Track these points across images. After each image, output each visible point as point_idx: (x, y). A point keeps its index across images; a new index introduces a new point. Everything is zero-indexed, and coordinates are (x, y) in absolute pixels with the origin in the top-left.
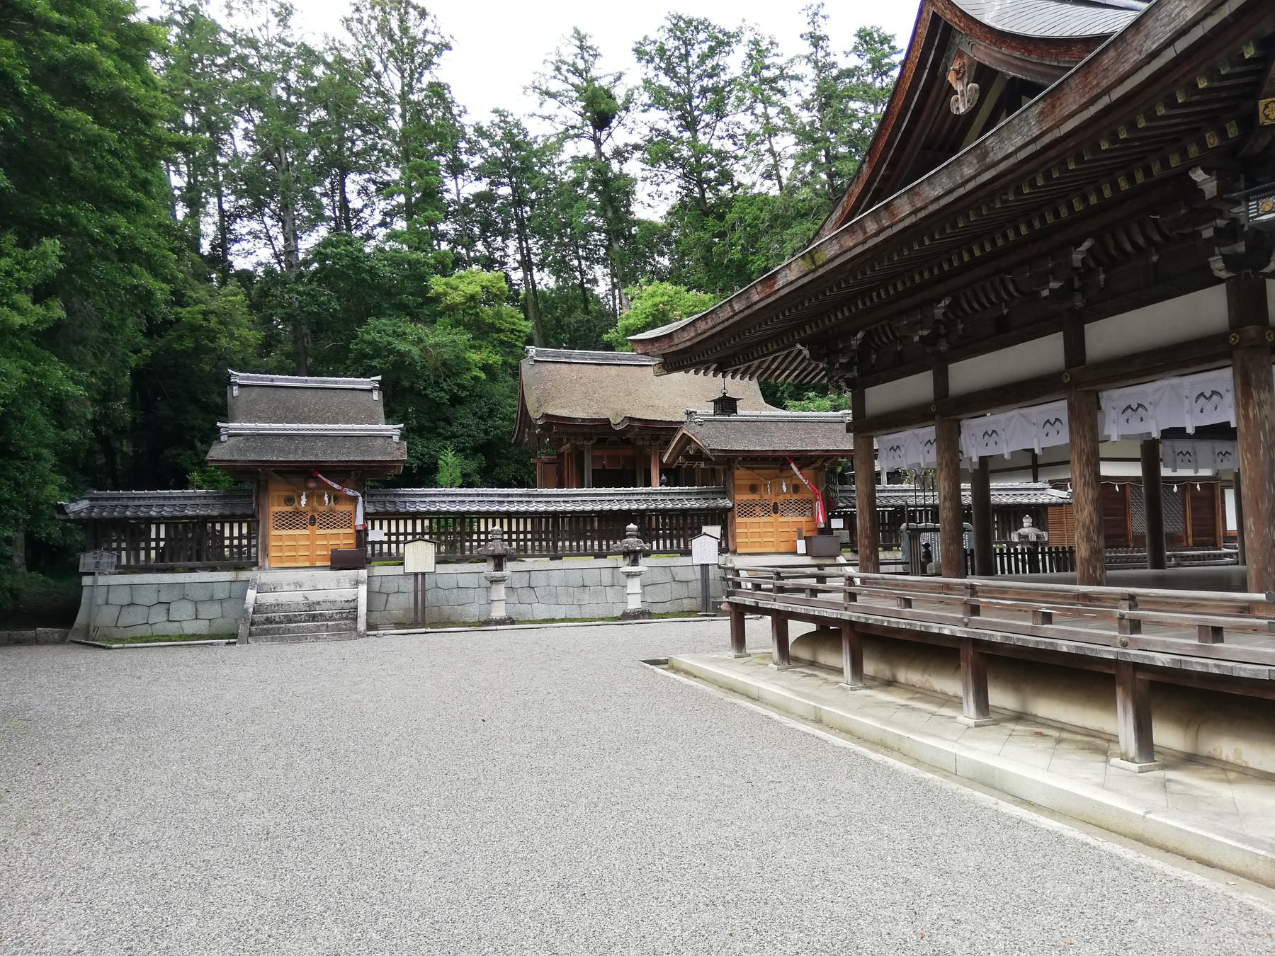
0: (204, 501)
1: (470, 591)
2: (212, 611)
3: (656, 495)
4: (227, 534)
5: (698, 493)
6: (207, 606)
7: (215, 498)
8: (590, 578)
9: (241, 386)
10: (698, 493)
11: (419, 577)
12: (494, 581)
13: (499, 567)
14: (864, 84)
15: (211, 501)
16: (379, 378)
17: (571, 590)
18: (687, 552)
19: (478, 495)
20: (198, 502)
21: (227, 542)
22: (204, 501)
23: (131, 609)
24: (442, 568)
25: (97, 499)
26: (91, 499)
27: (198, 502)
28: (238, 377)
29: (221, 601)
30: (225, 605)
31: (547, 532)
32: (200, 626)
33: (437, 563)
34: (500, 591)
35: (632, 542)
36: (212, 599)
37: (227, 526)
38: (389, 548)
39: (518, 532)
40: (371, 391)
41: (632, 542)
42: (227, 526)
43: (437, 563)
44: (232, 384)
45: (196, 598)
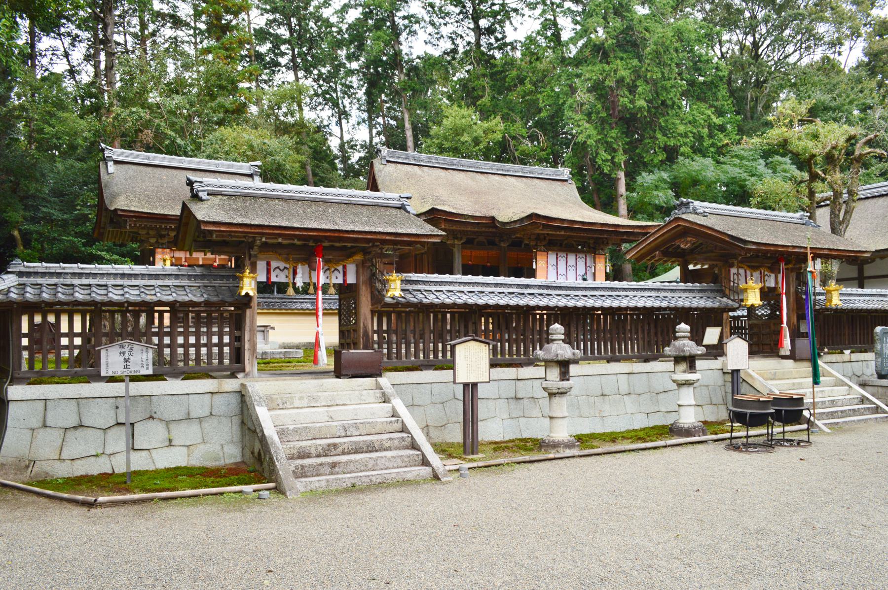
0: (177, 282)
1: (491, 403)
2: (186, 433)
3: (665, 289)
4: (64, 328)
5: (700, 291)
6: (183, 426)
7: (189, 277)
8: (524, 390)
9: (117, 162)
10: (700, 291)
11: (470, 389)
12: (681, 384)
13: (565, 375)
14: (347, 30)
15: (185, 282)
16: (258, 163)
17: (592, 399)
18: (450, 365)
19: (497, 285)
20: (167, 282)
21: (64, 341)
22: (177, 282)
23: (79, 433)
24: (499, 373)
25: (29, 274)
26: (20, 274)
27: (167, 282)
28: (117, 153)
29: (200, 419)
30: (205, 425)
31: (591, 331)
32: (175, 458)
33: (493, 365)
34: (561, 406)
35: (561, 349)
36: (188, 418)
37: (64, 320)
38: (198, 353)
39: (209, 345)
40: (251, 176)
41: (564, 351)
42: (64, 320)
43: (493, 365)
44: (105, 160)
45: (167, 417)
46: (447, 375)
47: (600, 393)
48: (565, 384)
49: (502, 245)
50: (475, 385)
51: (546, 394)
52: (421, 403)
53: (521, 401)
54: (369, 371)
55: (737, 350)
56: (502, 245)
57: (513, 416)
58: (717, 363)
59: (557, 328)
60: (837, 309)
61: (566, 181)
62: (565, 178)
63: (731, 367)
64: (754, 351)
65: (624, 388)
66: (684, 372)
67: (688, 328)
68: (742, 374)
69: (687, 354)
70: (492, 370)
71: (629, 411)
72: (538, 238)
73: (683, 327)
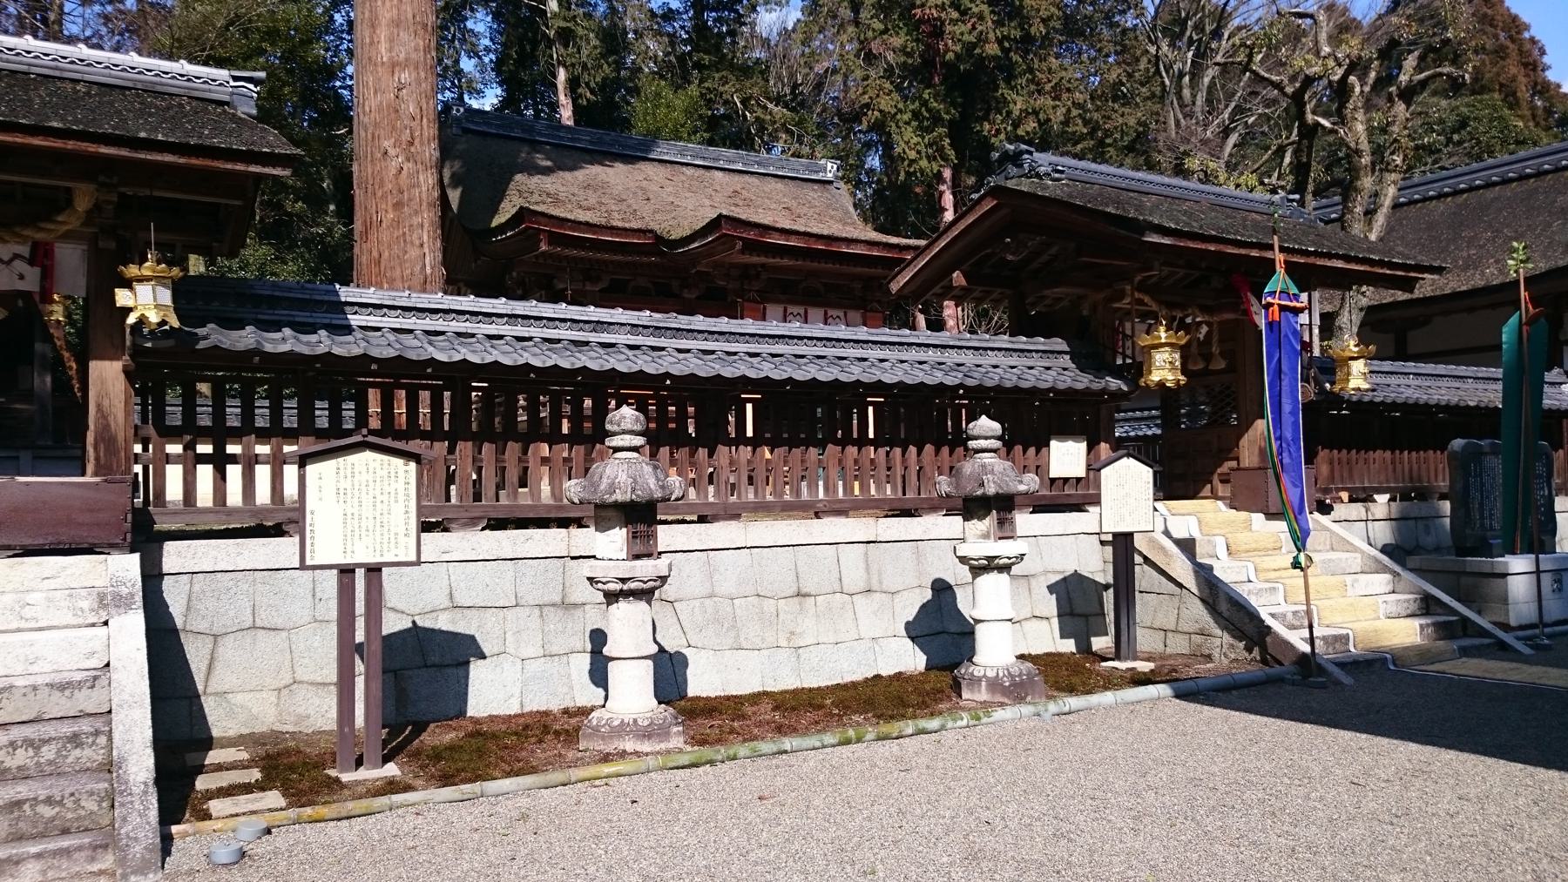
13: (643, 549)
19: (513, 318)
35: (625, 470)
46: (281, 550)
47: (794, 590)
48: (645, 569)
49: (686, 295)
50: (374, 570)
51: (600, 597)
52: (279, 622)
53: (578, 613)
54: (65, 537)
55: (1128, 487)
56: (686, 295)
57: (555, 649)
58: (1085, 521)
59: (627, 416)
60: (1360, 402)
61: (830, 182)
62: (830, 176)
63: (1113, 525)
64: (1171, 487)
65: (855, 578)
66: (986, 536)
67: (995, 427)
68: (1139, 542)
69: (991, 490)
70: (424, 535)
71: (867, 632)
72: (747, 272)
73: (986, 425)
